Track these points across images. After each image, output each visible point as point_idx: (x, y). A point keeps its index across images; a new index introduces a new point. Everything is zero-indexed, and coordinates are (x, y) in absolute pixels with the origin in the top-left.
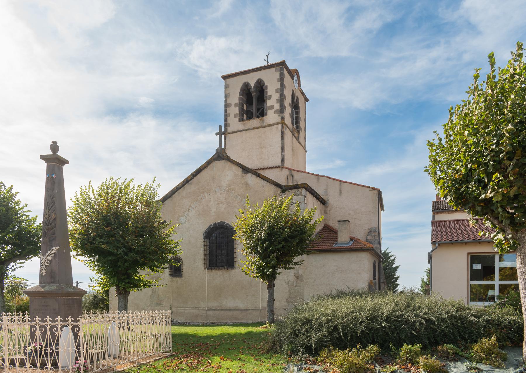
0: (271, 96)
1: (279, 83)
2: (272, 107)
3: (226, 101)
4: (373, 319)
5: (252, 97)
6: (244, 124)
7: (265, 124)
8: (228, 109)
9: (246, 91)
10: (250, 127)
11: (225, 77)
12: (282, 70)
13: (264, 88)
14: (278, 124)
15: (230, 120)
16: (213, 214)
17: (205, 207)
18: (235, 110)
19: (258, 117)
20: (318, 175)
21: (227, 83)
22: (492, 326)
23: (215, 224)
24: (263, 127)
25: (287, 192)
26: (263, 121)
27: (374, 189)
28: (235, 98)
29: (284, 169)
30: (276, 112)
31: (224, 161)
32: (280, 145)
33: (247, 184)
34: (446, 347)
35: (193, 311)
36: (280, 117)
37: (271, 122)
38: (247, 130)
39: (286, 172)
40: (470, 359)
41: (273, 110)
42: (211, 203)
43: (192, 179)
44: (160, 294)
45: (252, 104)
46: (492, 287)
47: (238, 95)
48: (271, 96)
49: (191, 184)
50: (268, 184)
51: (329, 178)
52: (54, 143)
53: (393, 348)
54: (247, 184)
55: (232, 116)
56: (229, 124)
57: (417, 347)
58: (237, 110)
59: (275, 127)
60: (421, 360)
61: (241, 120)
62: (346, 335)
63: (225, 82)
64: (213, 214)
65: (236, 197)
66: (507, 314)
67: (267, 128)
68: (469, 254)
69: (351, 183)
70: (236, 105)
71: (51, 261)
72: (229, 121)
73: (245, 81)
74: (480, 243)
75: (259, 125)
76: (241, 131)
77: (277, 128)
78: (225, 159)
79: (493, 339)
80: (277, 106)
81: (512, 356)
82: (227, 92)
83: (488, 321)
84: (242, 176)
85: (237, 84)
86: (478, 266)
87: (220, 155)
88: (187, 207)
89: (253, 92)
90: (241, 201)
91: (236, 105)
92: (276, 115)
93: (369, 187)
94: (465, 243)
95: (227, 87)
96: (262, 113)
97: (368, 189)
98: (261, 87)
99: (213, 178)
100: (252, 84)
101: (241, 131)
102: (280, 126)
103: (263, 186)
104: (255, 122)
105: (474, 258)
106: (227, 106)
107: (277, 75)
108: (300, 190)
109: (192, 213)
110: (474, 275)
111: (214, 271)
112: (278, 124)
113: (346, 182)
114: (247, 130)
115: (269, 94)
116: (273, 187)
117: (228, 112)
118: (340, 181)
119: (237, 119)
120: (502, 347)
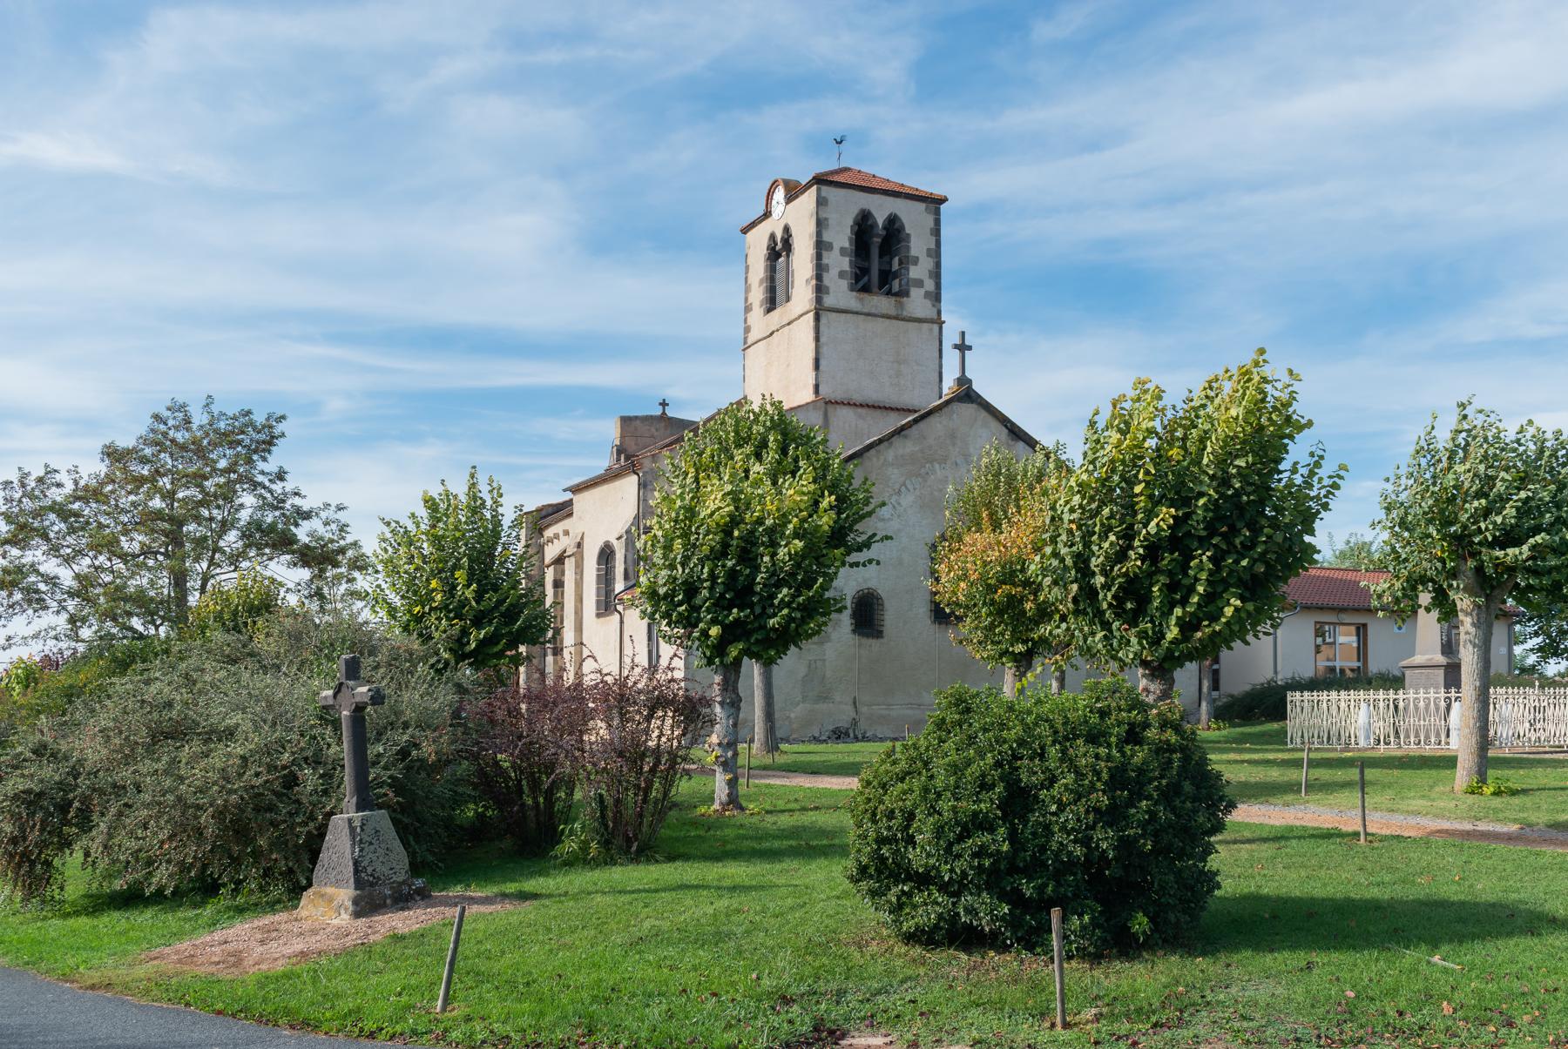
2: (919, 283)
3: (819, 234)
6: (861, 300)
8: (825, 254)
15: (830, 279)
21: (823, 194)
26: (901, 306)
28: (842, 237)
31: (974, 406)
35: (909, 712)
37: (919, 314)
41: (922, 291)
44: (828, 674)
52: (769, 310)
58: (845, 264)
59: (925, 325)
67: (911, 325)
70: (843, 251)
72: (826, 281)
73: (866, 207)
75: (893, 312)
88: (897, 486)
91: (843, 251)
92: (928, 303)
98: (895, 230)
99: (953, 436)
104: (881, 303)
109: (907, 500)
119: (844, 284)
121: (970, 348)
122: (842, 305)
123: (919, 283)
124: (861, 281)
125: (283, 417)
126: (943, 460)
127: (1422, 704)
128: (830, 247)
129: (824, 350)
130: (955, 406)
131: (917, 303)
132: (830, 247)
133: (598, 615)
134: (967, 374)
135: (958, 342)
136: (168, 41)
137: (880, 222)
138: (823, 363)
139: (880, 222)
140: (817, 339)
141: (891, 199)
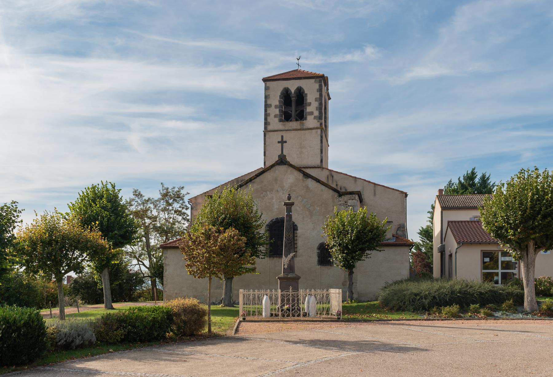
0: (311, 103)
1: (319, 93)
2: (311, 113)
3: (266, 102)
4: (453, 292)
5: (291, 101)
6: (284, 125)
7: (304, 127)
8: (268, 109)
9: (286, 95)
10: (290, 128)
11: (265, 80)
12: (320, 82)
13: (304, 95)
14: (317, 128)
15: (271, 119)
16: (276, 210)
17: (268, 204)
18: (275, 111)
19: (297, 120)
20: (355, 178)
21: (267, 85)
22: (510, 295)
23: (277, 219)
24: (303, 130)
25: (343, 197)
26: (303, 124)
27: (402, 192)
28: (276, 100)
29: (324, 170)
30: (315, 118)
31: (286, 166)
32: (320, 147)
33: (307, 187)
34: (490, 305)
36: (319, 123)
37: (311, 126)
38: (287, 130)
39: (326, 173)
40: (503, 310)
41: (313, 116)
42: (274, 201)
43: (255, 178)
45: (291, 106)
46: (497, 274)
47: (278, 98)
48: (311, 103)
49: (254, 182)
50: (327, 188)
51: (365, 180)
53: (466, 307)
54: (308, 187)
55: (272, 116)
56: (269, 123)
57: (477, 306)
58: (277, 111)
59: (314, 131)
60: (482, 311)
61: (281, 121)
62: (440, 300)
63: (266, 84)
64: (276, 210)
65: (297, 197)
66: (516, 289)
67: (307, 131)
68: (482, 251)
69: (384, 186)
70: (276, 107)
71: (290, 261)
72: (269, 120)
73: (286, 86)
74: (489, 244)
75: (299, 127)
76: (282, 131)
77: (317, 132)
78: (288, 165)
79: (511, 301)
80: (316, 113)
81: (519, 308)
82: (267, 94)
83: (507, 292)
84: (303, 180)
85: (278, 87)
86: (487, 260)
87: (282, 161)
89: (293, 97)
90: (302, 201)
91: (276, 107)
92: (316, 121)
93: (399, 191)
94: (480, 243)
95: (267, 89)
96: (301, 116)
97: (398, 192)
98: (301, 94)
99: (276, 180)
100: (293, 90)
101: (282, 131)
102: (319, 131)
103: (322, 190)
104: (294, 124)
105: (485, 254)
106: (267, 106)
107: (317, 86)
108: (354, 195)
110: (485, 266)
111: (275, 259)
112: (317, 128)
113: (379, 185)
114: (287, 130)
115: (309, 101)
116: (331, 192)
117: (268, 112)
118: (375, 184)
119: (277, 120)
120: (515, 305)
121: (286, 142)
122: (276, 128)
123: (311, 113)
124: (286, 117)
125: (183, 188)
126: (271, 190)
127: (251, 297)
128: (270, 106)
129: (267, 148)
130: (277, 167)
131: (311, 122)
132: (270, 106)
133: (482, 251)
134: (284, 153)
135: (280, 140)
136: (462, 20)
137: (293, 91)
138: (267, 153)
139: (293, 91)
140: (265, 144)
141: (298, 81)
